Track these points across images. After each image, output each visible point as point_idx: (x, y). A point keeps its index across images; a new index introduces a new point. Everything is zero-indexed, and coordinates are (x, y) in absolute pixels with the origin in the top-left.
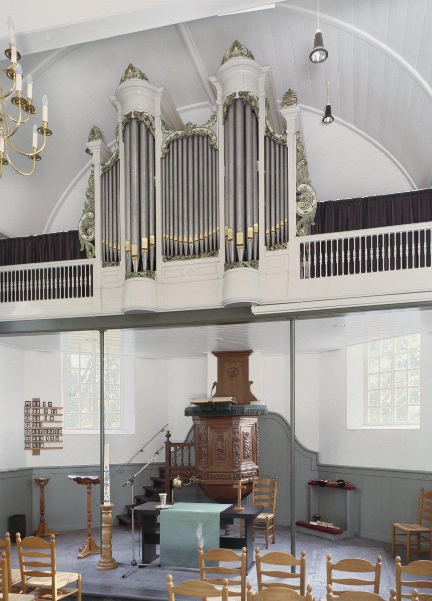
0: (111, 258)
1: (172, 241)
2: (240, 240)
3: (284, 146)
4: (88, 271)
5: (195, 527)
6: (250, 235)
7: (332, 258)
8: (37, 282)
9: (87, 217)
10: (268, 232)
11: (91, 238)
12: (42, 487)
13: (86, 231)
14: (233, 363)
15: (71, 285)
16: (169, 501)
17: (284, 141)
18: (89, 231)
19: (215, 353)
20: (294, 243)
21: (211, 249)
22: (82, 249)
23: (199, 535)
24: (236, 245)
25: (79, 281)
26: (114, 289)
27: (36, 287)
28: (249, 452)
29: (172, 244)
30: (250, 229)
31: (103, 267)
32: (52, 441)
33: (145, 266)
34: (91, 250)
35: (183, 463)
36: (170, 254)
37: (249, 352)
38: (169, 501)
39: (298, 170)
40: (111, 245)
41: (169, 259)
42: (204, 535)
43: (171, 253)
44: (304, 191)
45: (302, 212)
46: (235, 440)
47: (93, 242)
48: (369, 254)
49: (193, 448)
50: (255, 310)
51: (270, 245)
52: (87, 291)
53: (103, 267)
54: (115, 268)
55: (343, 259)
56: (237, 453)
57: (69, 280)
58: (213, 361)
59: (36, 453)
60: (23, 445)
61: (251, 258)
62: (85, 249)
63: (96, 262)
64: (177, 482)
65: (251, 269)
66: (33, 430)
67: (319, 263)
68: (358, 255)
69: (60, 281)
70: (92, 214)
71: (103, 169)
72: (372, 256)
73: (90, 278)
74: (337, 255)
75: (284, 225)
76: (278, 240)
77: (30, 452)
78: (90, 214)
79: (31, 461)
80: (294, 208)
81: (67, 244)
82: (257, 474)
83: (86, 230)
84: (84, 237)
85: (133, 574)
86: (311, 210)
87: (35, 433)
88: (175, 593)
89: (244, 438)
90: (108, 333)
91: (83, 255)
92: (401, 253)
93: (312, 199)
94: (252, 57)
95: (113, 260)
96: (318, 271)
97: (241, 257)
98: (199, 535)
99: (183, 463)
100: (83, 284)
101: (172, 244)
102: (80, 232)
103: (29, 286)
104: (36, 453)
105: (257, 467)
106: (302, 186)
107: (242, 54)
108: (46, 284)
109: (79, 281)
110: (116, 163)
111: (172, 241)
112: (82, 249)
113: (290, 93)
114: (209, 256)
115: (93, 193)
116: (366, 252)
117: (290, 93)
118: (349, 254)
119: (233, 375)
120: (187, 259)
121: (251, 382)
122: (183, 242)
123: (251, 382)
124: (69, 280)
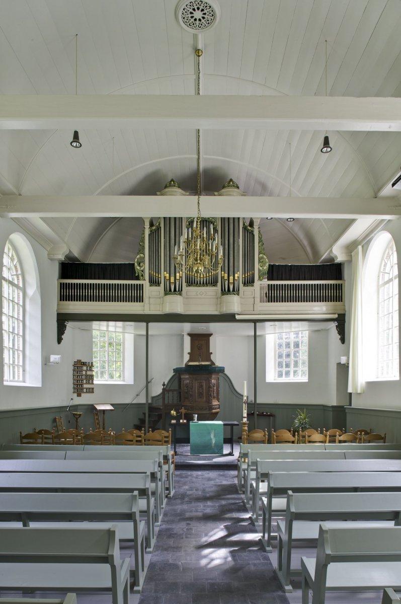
0: (154, 282)
2: (172, 280)
3: (252, 234)
4: (141, 287)
5: (209, 434)
6: (178, 278)
8: (107, 291)
9: (140, 257)
10: (244, 276)
11: (142, 269)
12: (77, 419)
13: (139, 264)
14: (201, 343)
15: (66, 294)
16: (199, 419)
17: (252, 231)
18: (141, 264)
19: (189, 335)
20: (257, 283)
21: (214, 283)
22: (137, 275)
23: (212, 436)
24: (170, 283)
25: (134, 293)
26: (154, 300)
27: (97, 292)
28: (215, 395)
30: (178, 274)
31: (150, 286)
32: (89, 383)
33: (173, 290)
34: (142, 276)
35: (168, 402)
36: (190, 283)
37: (211, 334)
38: (199, 419)
39: (259, 247)
40: (154, 274)
41: (189, 286)
42: (214, 436)
43: (191, 282)
44: (262, 258)
45: (261, 268)
46: (210, 387)
48: (123, 293)
49: (175, 393)
50: (237, 317)
51: (245, 284)
52: (140, 299)
53: (150, 286)
54: (214, 288)
56: (211, 395)
57: (324, 292)
58: (187, 341)
59: (79, 395)
61: (178, 291)
62: (138, 275)
63: (146, 283)
64: (173, 413)
67: (272, 296)
69: (103, 294)
70: (143, 255)
71: (151, 231)
72: (284, 294)
73: (141, 292)
74: (335, 294)
75: (252, 274)
76: (249, 282)
77: (76, 394)
78: (142, 255)
79: (78, 401)
80: (257, 266)
81: (127, 271)
82: (219, 408)
84: (138, 268)
86: (266, 268)
87: (77, 382)
89: (214, 386)
90: (150, 324)
91: (137, 278)
92: (303, 294)
93: (266, 263)
94: (238, 188)
95: (156, 283)
97: (173, 289)
98: (212, 436)
99: (168, 402)
100: (331, 294)
102: (136, 264)
104: (79, 395)
105: (219, 403)
106: (261, 255)
107: (233, 186)
108: (288, 293)
109: (134, 293)
110: (159, 228)
112: (137, 275)
114: (212, 286)
115: (144, 243)
116: (281, 292)
119: (200, 348)
120: (199, 286)
121: (212, 353)
123: (212, 353)
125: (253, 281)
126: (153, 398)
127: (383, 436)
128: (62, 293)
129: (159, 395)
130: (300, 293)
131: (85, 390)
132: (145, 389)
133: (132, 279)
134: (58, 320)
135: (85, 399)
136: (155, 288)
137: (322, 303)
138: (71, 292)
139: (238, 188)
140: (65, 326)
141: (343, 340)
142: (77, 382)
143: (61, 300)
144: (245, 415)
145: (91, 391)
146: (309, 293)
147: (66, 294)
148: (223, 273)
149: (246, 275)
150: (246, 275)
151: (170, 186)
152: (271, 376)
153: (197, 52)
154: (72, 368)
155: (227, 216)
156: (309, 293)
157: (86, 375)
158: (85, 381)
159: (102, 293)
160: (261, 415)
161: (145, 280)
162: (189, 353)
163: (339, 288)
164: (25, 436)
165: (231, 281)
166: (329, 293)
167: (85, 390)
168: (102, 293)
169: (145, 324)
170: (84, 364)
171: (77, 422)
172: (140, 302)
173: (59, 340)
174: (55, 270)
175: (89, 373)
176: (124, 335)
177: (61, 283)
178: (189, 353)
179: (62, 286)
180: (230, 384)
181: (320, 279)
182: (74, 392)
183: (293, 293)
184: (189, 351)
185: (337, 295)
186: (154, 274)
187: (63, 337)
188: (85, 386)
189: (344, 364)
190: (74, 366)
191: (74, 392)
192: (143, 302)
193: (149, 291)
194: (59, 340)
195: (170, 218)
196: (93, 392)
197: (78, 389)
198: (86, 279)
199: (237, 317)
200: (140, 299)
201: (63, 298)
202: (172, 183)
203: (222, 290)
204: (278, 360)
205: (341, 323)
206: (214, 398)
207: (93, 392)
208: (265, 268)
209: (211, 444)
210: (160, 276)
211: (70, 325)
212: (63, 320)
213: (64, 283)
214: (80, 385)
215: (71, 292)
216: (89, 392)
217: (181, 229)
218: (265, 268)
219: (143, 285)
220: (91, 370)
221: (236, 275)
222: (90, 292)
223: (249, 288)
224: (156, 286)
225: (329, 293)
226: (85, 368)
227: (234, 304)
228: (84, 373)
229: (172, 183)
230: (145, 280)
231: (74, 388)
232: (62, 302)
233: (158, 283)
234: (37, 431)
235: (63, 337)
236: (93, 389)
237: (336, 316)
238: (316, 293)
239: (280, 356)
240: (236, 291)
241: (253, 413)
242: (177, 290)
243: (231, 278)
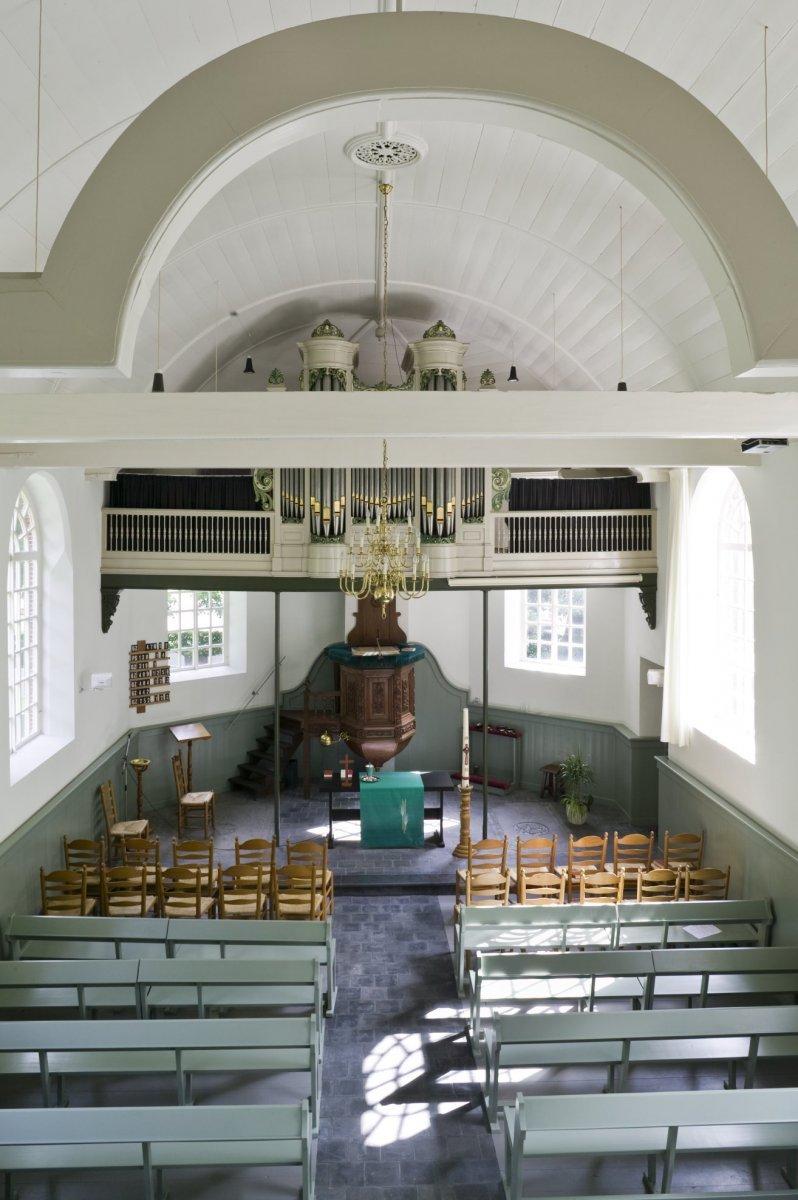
0: (291, 515)
1: (296, 506)
5: (398, 807)
7: (531, 535)
8: (615, 530)
10: (464, 503)
11: (267, 488)
13: (262, 480)
18: (266, 480)
20: (490, 517)
22: (257, 500)
23: (403, 813)
24: (322, 520)
25: (252, 535)
27: (180, 532)
29: (362, 504)
32: (160, 683)
34: (268, 502)
40: (292, 499)
42: (408, 811)
46: (396, 692)
47: (271, 493)
50: (451, 583)
52: (263, 547)
55: (550, 537)
59: (141, 710)
60: (128, 702)
62: (261, 500)
63: (275, 517)
65: (451, 544)
66: (139, 673)
67: (521, 540)
68: (200, 534)
76: (474, 514)
77: (134, 709)
83: (263, 478)
84: (260, 486)
85: (374, 1124)
86: (506, 486)
88: (339, 986)
89: (404, 688)
90: (283, 595)
91: (259, 507)
96: (516, 546)
101: (362, 504)
102: (255, 480)
103: (178, 534)
104: (141, 710)
109: (252, 535)
111: (296, 506)
112: (257, 500)
113: (487, 373)
117: (487, 373)
118: (540, 533)
121: (399, 614)
122: (374, 503)
123: (399, 614)
124: (519, 538)
125: (481, 513)
126: (286, 694)
127: (724, 871)
128: (111, 536)
129: (298, 689)
130: (574, 534)
131: (152, 699)
132: (274, 674)
133: (249, 508)
134: (104, 588)
135: (155, 715)
136: (291, 527)
137: (616, 554)
138: (131, 533)
139: (454, 336)
140: (116, 599)
141: (652, 622)
142: (138, 686)
143: (108, 549)
144: (466, 773)
145: (164, 698)
146: (589, 534)
147: (118, 537)
148: (424, 498)
149: (469, 501)
150: (469, 501)
151: (323, 333)
152: (514, 655)
153: (383, 188)
154: (128, 658)
155: (431, 465)
156: (589, 534)
157: (155, 670)
158: (152, 681)
159: (189, 534)
160: (496, 731)
161: (272, 510)
162: (355, 614)
163: (646, 523)
164: (51, 874)
165: (440, 515)
166: (626, 533)
167: (152, 699)
168: (189, 534)
169: (272, 595)
170: (151, 647)
171: (139, 779)
172: (263, 552)
173: (106, 625)
174: (99, 496)
175: (160, 664)
176: (229, 617)
177: (109, 516)
178: (355, 614)
179: (111, 521)
180: (434, 665)
181: (607, 510)
182: (131, 706)
183: (558, 534)
184: (356, 610)
185: (639, 536)
186: (292, 499)
187: (112, 618)
188: (154, 690)
189: (655, 686)
190: (132, 653)
191: (131, 706)
192: (268, 552)
193: (282, 532)
194: (106, 625)
195: (322, 470)
196: (168, 700)
197: (140, 698)
198: (163, 513)
199: (451, 583)
200: (263, 547)
201: (113, 544)
202: (327, 328)
203: (422, 531)
204: (527, 641)
205: (650, 590)
206: (404, 709)
207: (168, 700)
208: (505, 486)
209: (401, 825)
210: (302, 503)
211: (125, 595)
212: (111, 588)
213: (114, 516)
214: (142, 690)
215: (131, 533)
216: (161, 700)
217: (343, 479)
218: (505, 486)
219: (268, 519)
220: (164, 657)
221: (449, 505)
222: (167, 533)
223: (474, 527)
224: (295, 522)
225: (626, 533)
226: (152, 655)
227: (445, 559)
228: (151, 664)
229: (327, 328)
230: (272, 510)
231: (132, 698)
232: (111, 553)
233: (299, 517)
234: (68, 842)
235: (112, 618)
236: (167, 694)
237: (639, 579)
238: (602, 534)
239: (531, 633)
240: (448, 535)
241: (481, 727)
242: (336, 532)
243: (440, 511)
